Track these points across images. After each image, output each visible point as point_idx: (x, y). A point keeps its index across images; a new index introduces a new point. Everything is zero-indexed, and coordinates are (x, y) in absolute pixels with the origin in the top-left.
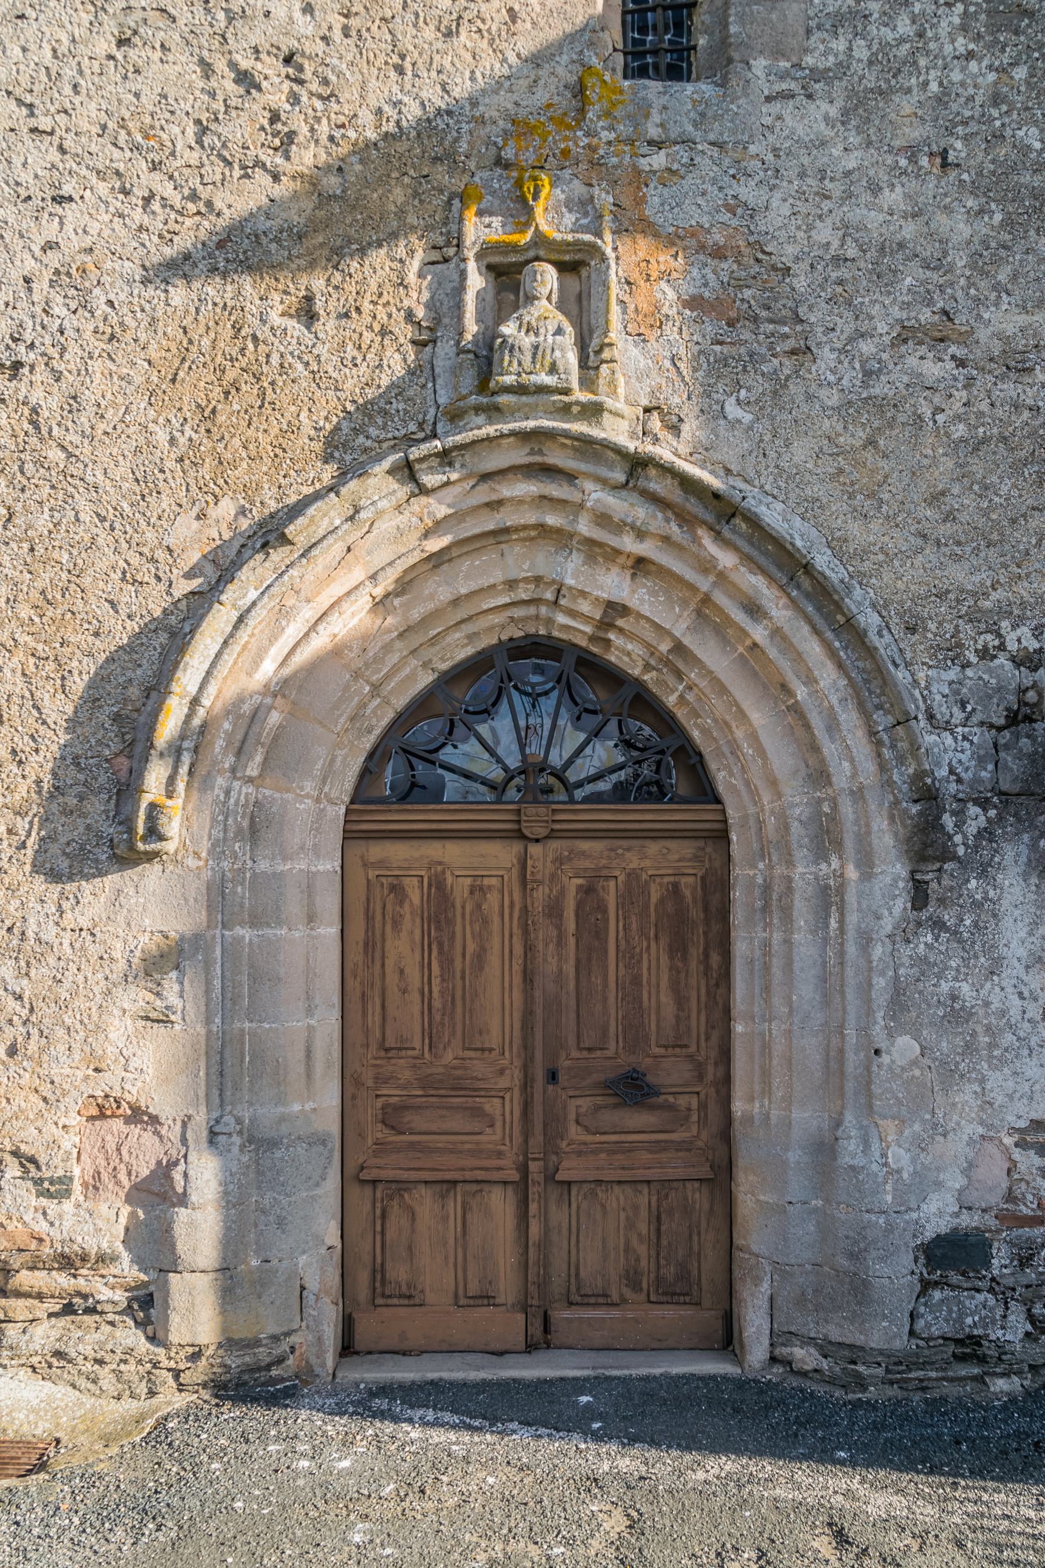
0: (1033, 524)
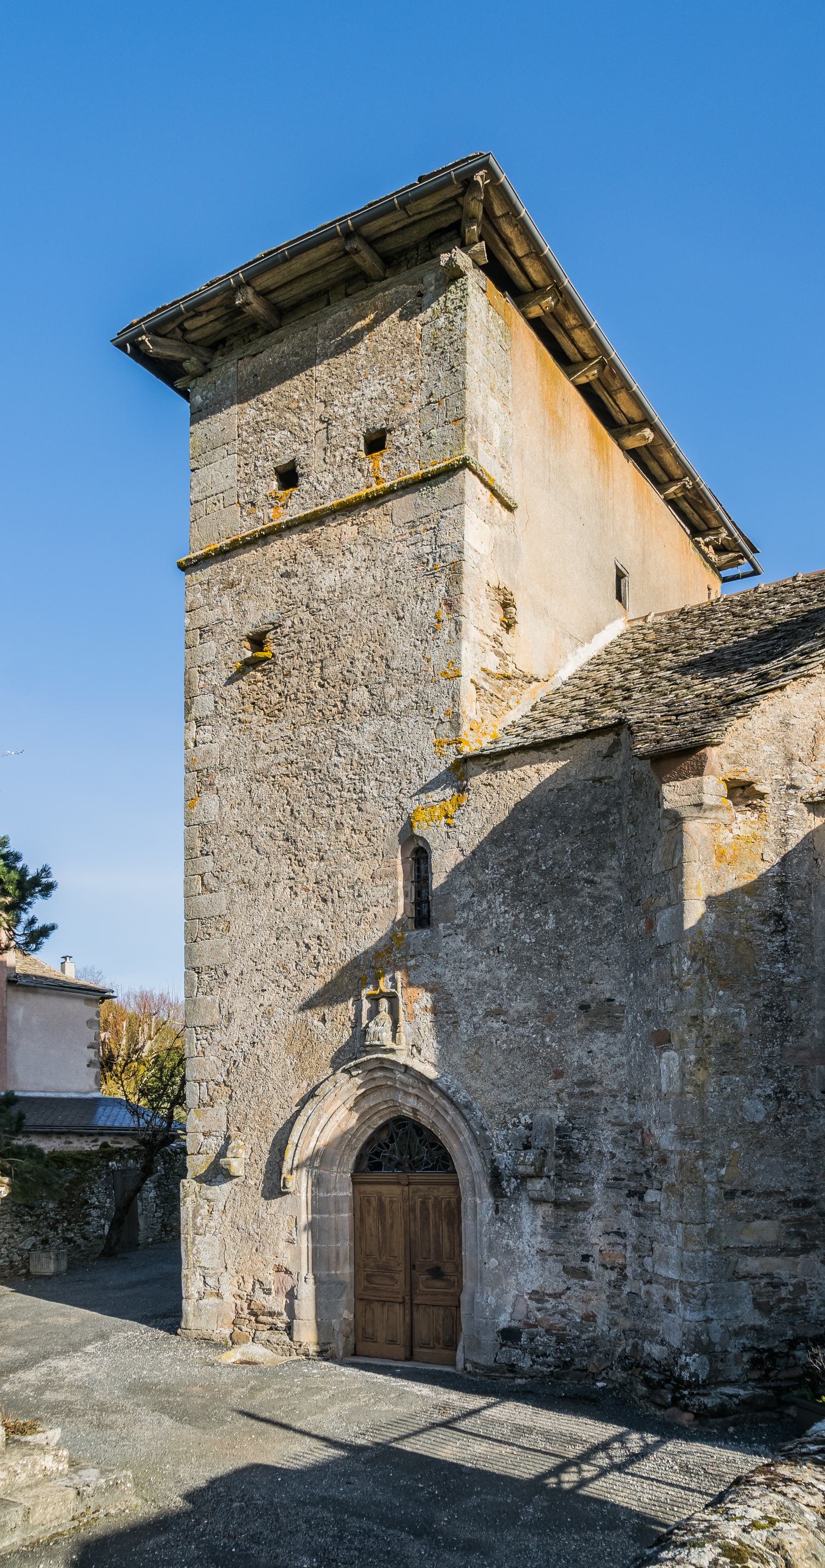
0: (529, 1078)
